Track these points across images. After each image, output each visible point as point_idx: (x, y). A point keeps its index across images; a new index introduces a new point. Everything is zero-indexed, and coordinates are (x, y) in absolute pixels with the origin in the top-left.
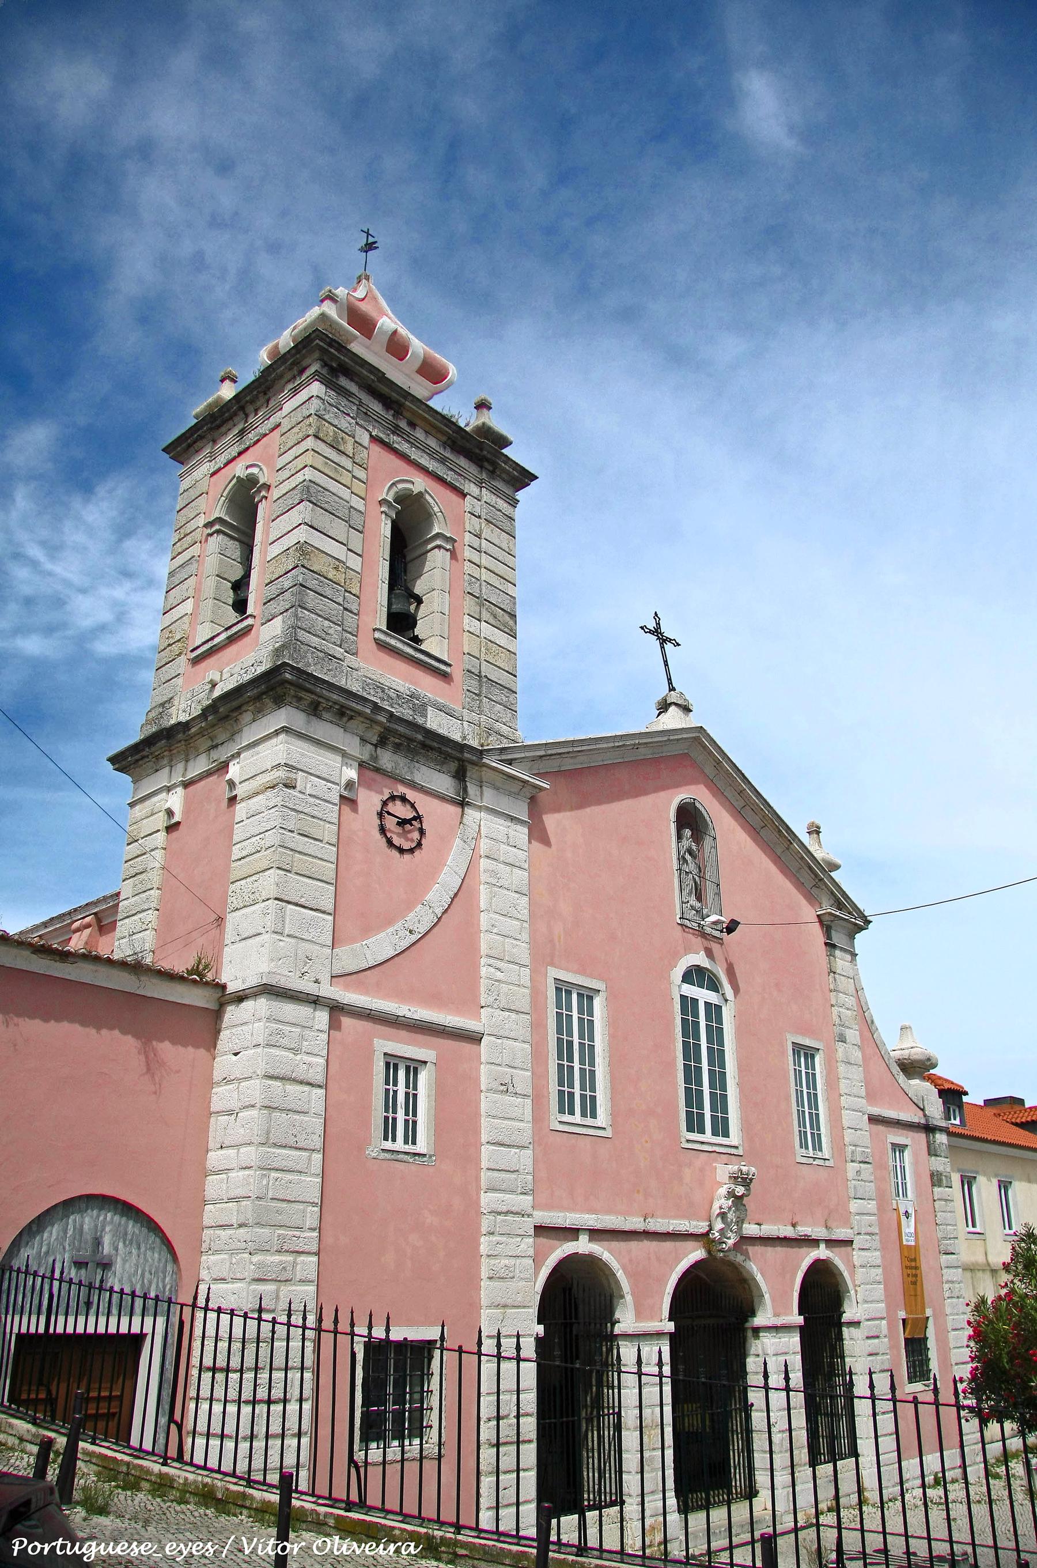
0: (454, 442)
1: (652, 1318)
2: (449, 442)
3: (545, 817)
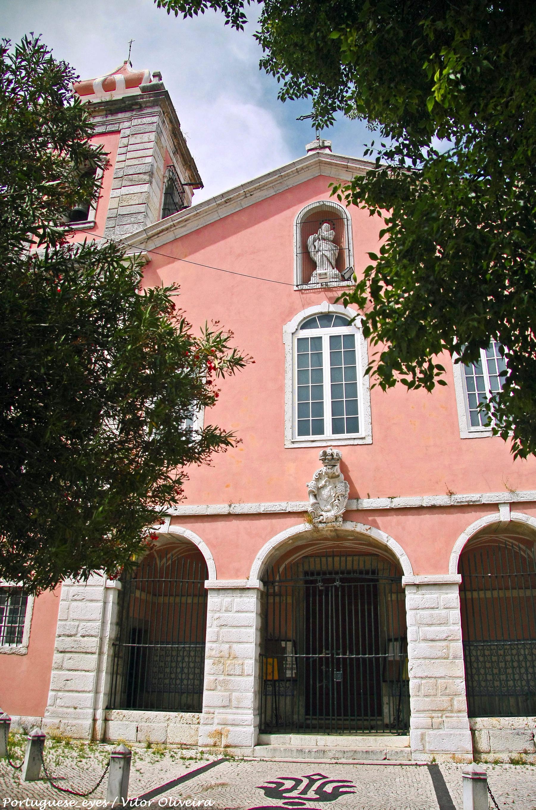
0: (110, 110)
1: (237, 576)
2: (108, 112)
3: (158, 271)
